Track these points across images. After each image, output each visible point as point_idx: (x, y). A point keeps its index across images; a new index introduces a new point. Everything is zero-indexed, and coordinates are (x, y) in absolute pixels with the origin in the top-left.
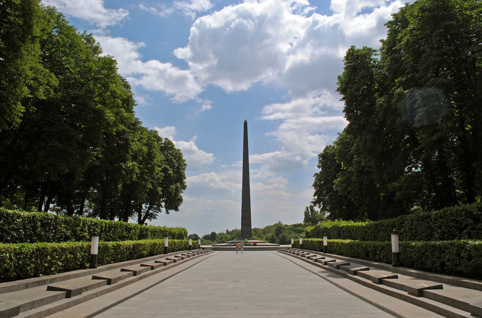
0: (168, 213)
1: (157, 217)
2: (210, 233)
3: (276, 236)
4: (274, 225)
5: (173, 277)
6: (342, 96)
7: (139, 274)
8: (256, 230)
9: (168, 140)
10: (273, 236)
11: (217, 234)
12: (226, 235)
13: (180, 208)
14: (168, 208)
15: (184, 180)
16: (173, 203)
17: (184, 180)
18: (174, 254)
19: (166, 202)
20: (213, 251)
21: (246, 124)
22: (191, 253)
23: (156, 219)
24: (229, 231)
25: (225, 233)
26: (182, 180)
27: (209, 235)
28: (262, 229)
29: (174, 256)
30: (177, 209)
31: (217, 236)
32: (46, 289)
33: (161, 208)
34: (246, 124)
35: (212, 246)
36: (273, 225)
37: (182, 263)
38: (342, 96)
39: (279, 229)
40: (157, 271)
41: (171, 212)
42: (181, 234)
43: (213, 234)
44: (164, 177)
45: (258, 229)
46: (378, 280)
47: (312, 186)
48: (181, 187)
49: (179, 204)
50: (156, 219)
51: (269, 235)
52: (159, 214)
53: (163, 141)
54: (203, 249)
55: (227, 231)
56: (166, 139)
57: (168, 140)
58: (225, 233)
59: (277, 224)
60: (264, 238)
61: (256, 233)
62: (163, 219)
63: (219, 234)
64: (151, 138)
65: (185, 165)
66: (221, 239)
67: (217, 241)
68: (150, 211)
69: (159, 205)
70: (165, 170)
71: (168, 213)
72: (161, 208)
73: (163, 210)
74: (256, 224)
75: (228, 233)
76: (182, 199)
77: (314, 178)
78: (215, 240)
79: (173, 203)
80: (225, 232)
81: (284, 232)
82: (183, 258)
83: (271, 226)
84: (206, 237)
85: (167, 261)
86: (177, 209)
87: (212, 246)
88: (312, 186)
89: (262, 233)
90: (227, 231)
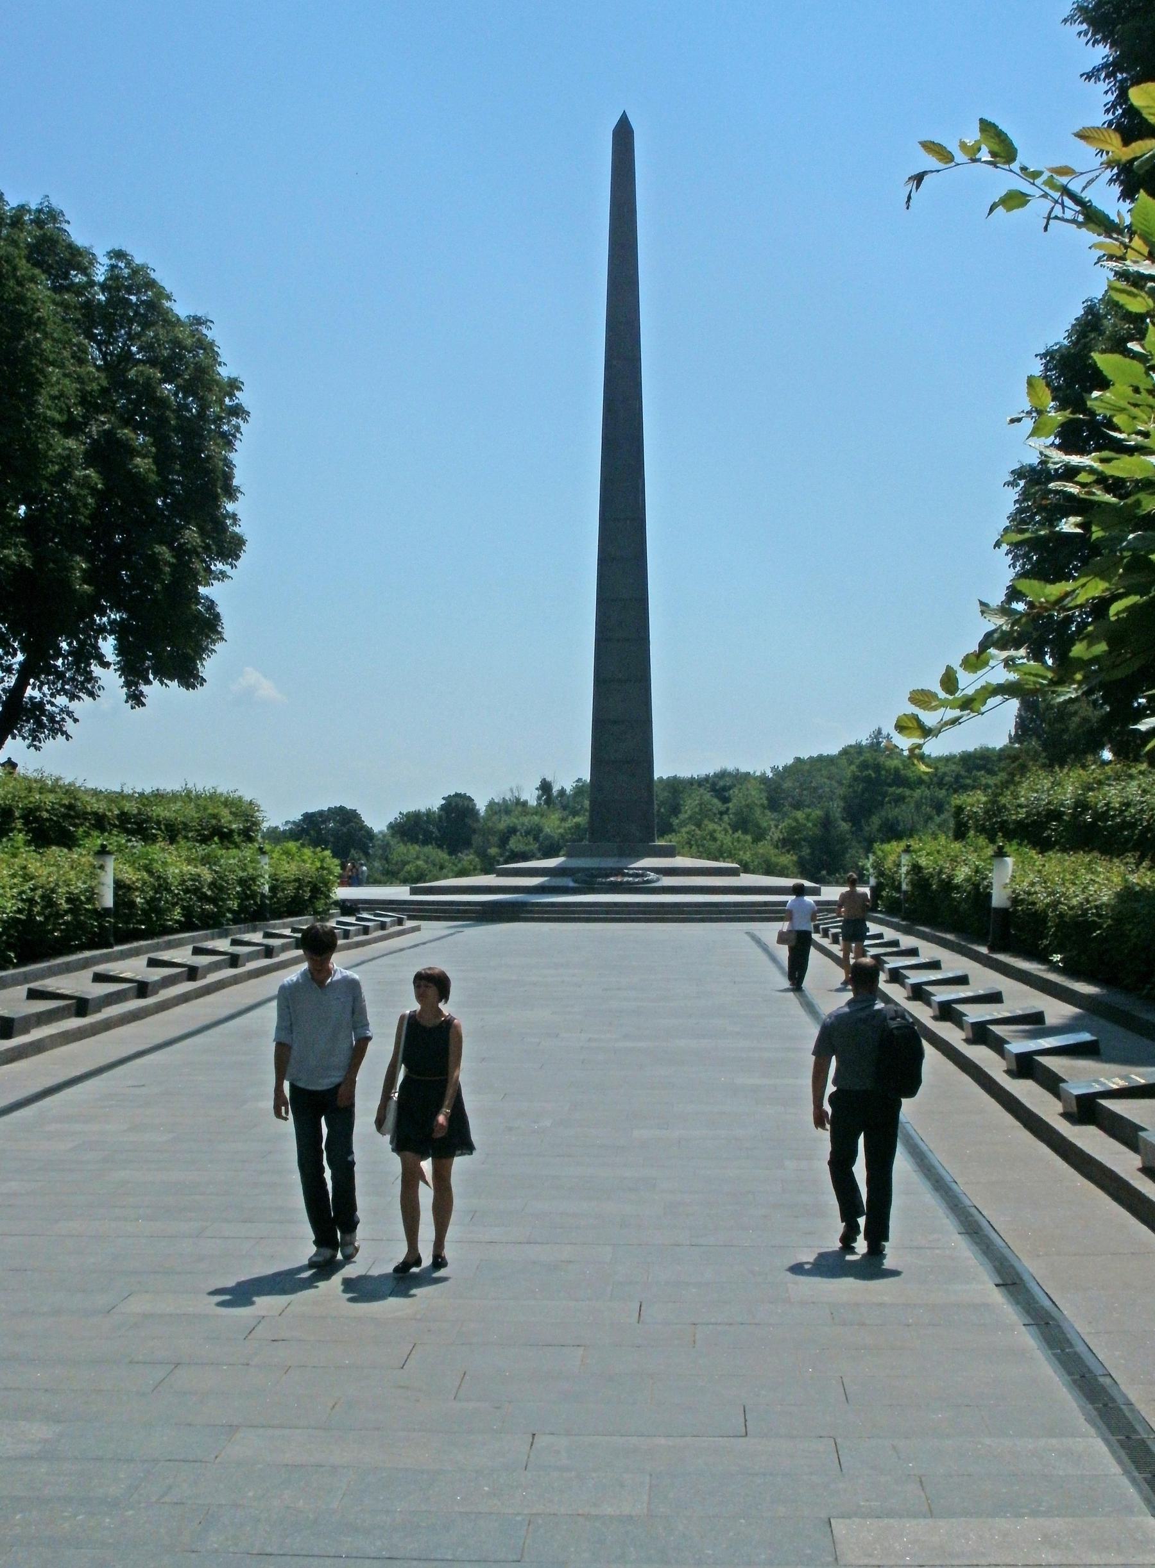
0: (136, 699)
1: (69, 725)
2: (433, 802)
3: (845, 826)
4: (845, 752)
5: (105, 1075)
6: (1102, 53)
7: (98, 1010)
8: (676, 786)
9: (128, 264)
10: (826, 823)
11: (481, 806)
12: (536, 811)
13: (208, 667)
14: (134, 673)
15: (230, 507)
16: (170, 641)
17: (230, 507)
18: (26, 978)
19: (120, 630)
20: (409, 924)
21: (623, 135)
22: (287, 932)
23: (68, 737)
24: (556, 789)
25: (533, 802)
26: (213, 501)
27: (429, 813)
28: (763, 779)
29: (142, 961)
30: (189, 676)
31: (477, 821)
32: (145, 963)
33: (96, 670)
34: (623, 135)
35: (414, 891)
36: (833, 750)
37: (185, 998)
38: (1102, 53)
39: (868, 780)
40: (32, 1044)
41: (160, 692)
42: (222, 825)
43: (458, 810)
44: (103, 497)
45: (741, 778)
46: (1074, 1102)
47: (998, 545)
48: (207, 548)
49: (200, 651)
50: (68, 737)
51: (800, 815)
52: (82, 706)
53: (100, 274)
54: (348, 907)
55: (545, 787)
56: (119, 255)
57: (128, 264)
58: (533, 802)
59: (858, 748)
60: (775, 834)
61: (726, 800)
62: (112, 739)
63: (491, 805)
64: (15, 269)
65: (237, 411)
66: (504, 840)
67: (482, 854)
68: (29, 692)
69: (86, 654)
70: (108, 454)
71: (136, 699)
72: (96, 670)
73: (110, 679)
74: (679, 752)
75: (549, 802)
76: (217, 616)
77: (1013, 494)
78: (467, 844)
79: (170, 641)
80: (531, 796)
81: (900, 799)
82: (269, 952)
83: (821, 758)
84: (411, 828)
85: (156, 975)
86: (189, 676)
87: (414, 891)
88: (998, 545)
89: (730, 809)
90: (545, 787)
